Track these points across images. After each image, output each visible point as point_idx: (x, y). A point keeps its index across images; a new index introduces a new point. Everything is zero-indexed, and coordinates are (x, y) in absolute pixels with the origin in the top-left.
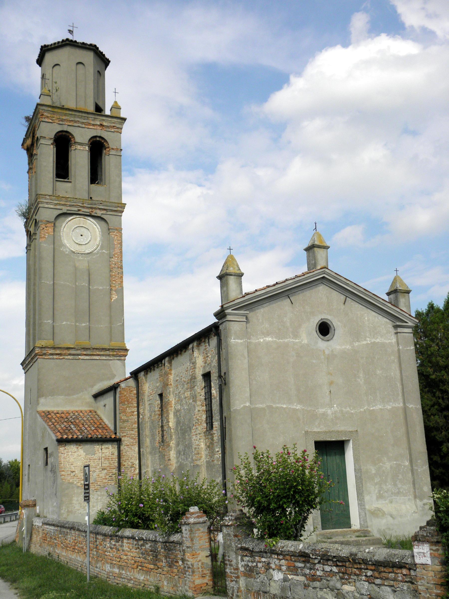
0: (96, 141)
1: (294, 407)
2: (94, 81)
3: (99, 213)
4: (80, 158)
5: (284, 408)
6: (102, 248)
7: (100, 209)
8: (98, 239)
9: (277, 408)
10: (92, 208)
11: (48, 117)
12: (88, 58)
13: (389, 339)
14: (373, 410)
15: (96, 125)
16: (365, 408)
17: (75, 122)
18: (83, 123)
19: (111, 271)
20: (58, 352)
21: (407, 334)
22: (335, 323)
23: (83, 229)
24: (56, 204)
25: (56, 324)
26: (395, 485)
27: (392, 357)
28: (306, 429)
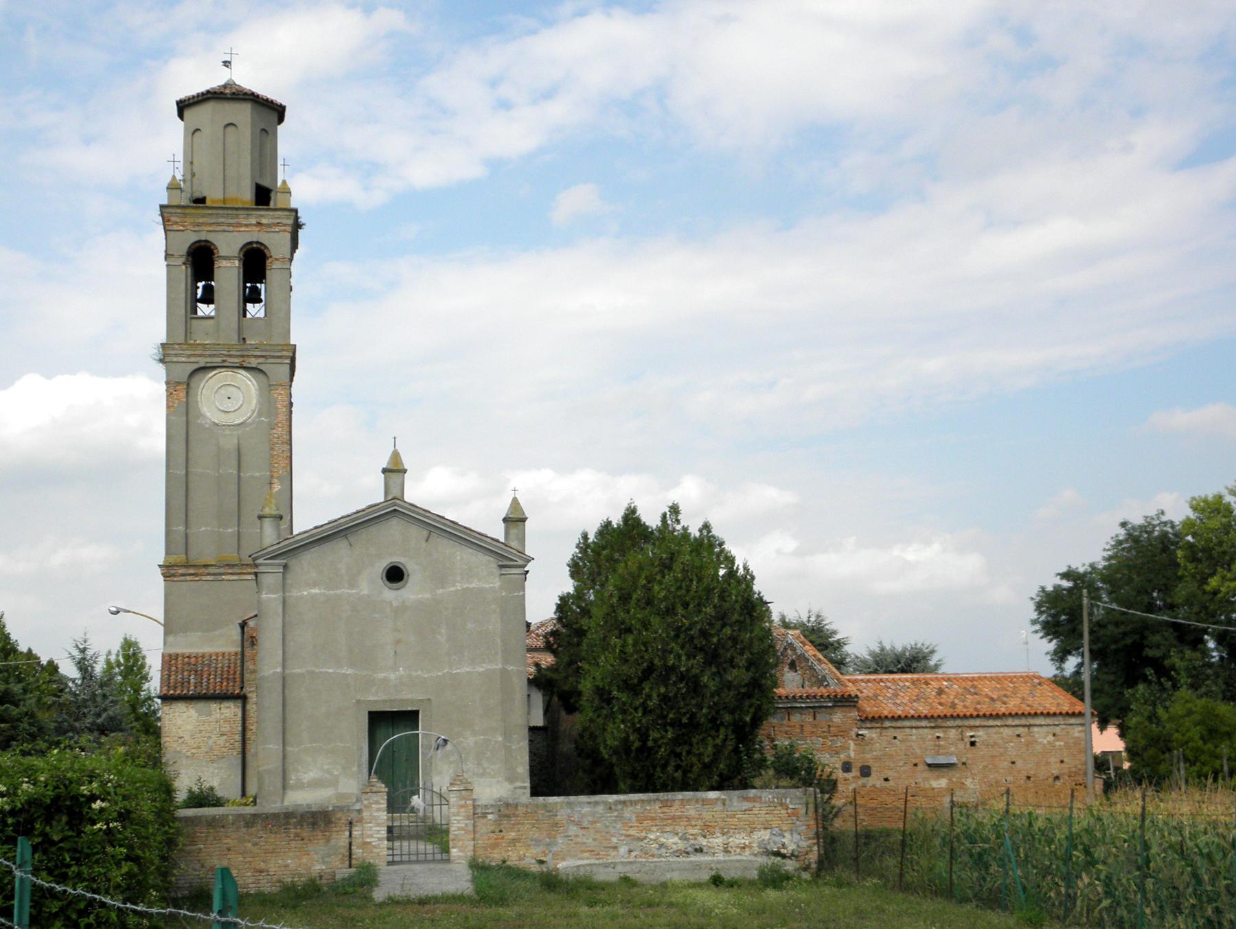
0: (253, 249)
2: (252, 148)
3: (254, 362)
4: (228, 274)
6: (260, 415)
7: (255, 356)
8: (254, 401)
10: (242, 356)
11: (176, 223)
12: (243, 113)
15: (251, 225)
17: (219, 224)
18: (230, 225)
19: (272, 449)
20: (192, 571)
22: (409, 566)
23: (231, 389)
24: (189, 356)
25: (191, 531)
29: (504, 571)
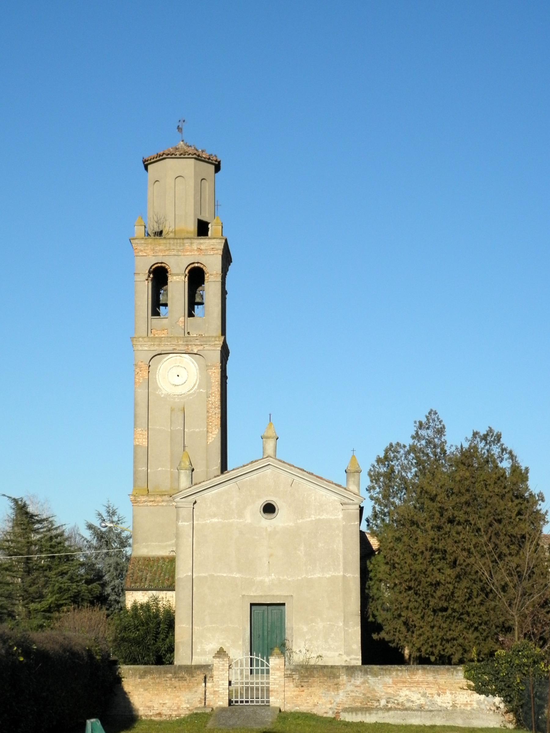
1: (234, 575)
5: (225, 577)
6: (200, 387)
9: (218, 576)
11: (141, 251)
13: (336, 515)
14: (311, 578)
16: (303, 576)
21: (353, 511)
26: (326, 642)
27: (337, 532)
28: (244, 593)
29: (345, 507)
